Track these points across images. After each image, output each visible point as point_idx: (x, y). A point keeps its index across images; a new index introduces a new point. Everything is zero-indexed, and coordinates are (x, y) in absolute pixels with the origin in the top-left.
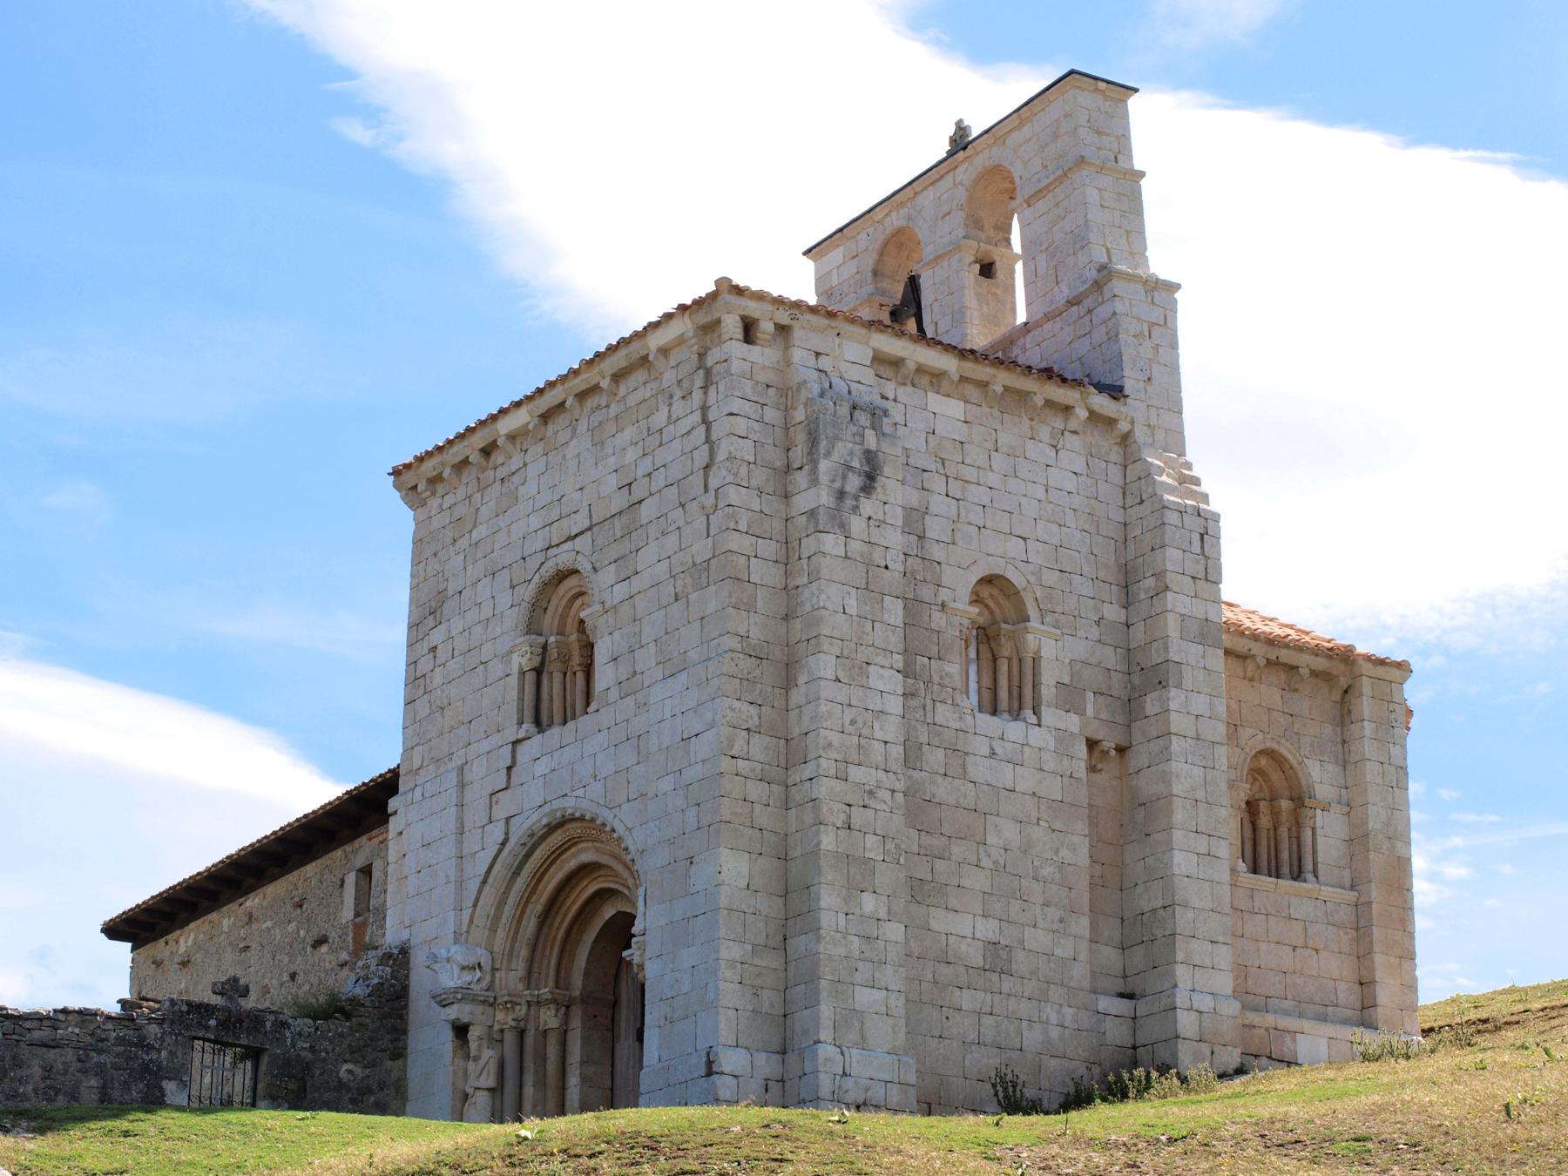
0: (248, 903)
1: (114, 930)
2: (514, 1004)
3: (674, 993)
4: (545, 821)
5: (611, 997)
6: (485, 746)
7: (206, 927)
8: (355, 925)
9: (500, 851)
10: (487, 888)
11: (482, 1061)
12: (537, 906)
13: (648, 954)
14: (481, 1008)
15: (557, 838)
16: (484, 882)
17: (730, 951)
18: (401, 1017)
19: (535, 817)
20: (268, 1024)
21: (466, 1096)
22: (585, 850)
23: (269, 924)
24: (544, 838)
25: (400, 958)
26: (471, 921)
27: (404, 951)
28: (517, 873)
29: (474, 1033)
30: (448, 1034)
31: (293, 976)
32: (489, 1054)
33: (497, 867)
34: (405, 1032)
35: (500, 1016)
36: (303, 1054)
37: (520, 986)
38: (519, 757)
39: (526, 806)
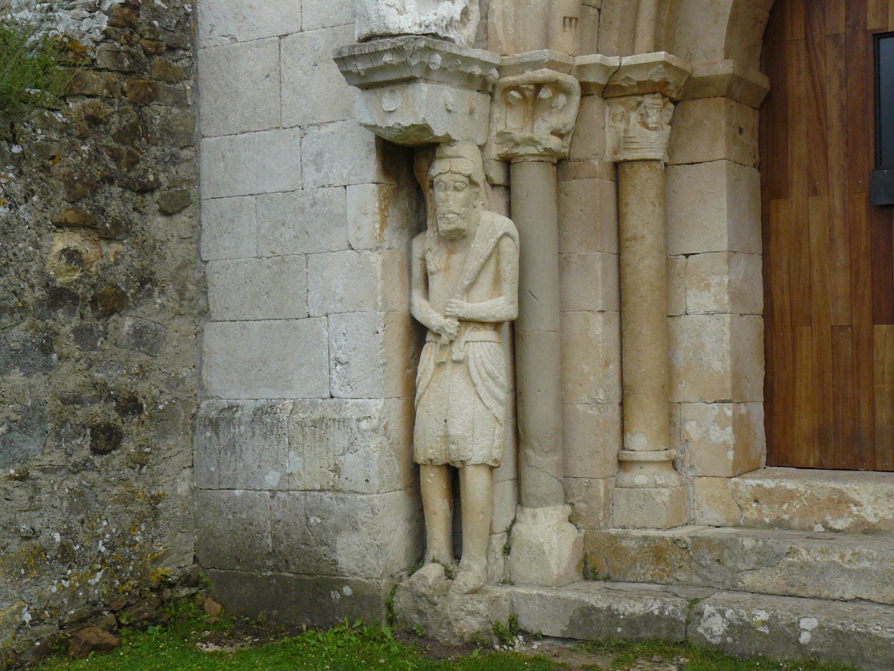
2: (558, 87)
11: (480, 247)
18: (180, 101)
35: (511, 122)
37: (565, 44)
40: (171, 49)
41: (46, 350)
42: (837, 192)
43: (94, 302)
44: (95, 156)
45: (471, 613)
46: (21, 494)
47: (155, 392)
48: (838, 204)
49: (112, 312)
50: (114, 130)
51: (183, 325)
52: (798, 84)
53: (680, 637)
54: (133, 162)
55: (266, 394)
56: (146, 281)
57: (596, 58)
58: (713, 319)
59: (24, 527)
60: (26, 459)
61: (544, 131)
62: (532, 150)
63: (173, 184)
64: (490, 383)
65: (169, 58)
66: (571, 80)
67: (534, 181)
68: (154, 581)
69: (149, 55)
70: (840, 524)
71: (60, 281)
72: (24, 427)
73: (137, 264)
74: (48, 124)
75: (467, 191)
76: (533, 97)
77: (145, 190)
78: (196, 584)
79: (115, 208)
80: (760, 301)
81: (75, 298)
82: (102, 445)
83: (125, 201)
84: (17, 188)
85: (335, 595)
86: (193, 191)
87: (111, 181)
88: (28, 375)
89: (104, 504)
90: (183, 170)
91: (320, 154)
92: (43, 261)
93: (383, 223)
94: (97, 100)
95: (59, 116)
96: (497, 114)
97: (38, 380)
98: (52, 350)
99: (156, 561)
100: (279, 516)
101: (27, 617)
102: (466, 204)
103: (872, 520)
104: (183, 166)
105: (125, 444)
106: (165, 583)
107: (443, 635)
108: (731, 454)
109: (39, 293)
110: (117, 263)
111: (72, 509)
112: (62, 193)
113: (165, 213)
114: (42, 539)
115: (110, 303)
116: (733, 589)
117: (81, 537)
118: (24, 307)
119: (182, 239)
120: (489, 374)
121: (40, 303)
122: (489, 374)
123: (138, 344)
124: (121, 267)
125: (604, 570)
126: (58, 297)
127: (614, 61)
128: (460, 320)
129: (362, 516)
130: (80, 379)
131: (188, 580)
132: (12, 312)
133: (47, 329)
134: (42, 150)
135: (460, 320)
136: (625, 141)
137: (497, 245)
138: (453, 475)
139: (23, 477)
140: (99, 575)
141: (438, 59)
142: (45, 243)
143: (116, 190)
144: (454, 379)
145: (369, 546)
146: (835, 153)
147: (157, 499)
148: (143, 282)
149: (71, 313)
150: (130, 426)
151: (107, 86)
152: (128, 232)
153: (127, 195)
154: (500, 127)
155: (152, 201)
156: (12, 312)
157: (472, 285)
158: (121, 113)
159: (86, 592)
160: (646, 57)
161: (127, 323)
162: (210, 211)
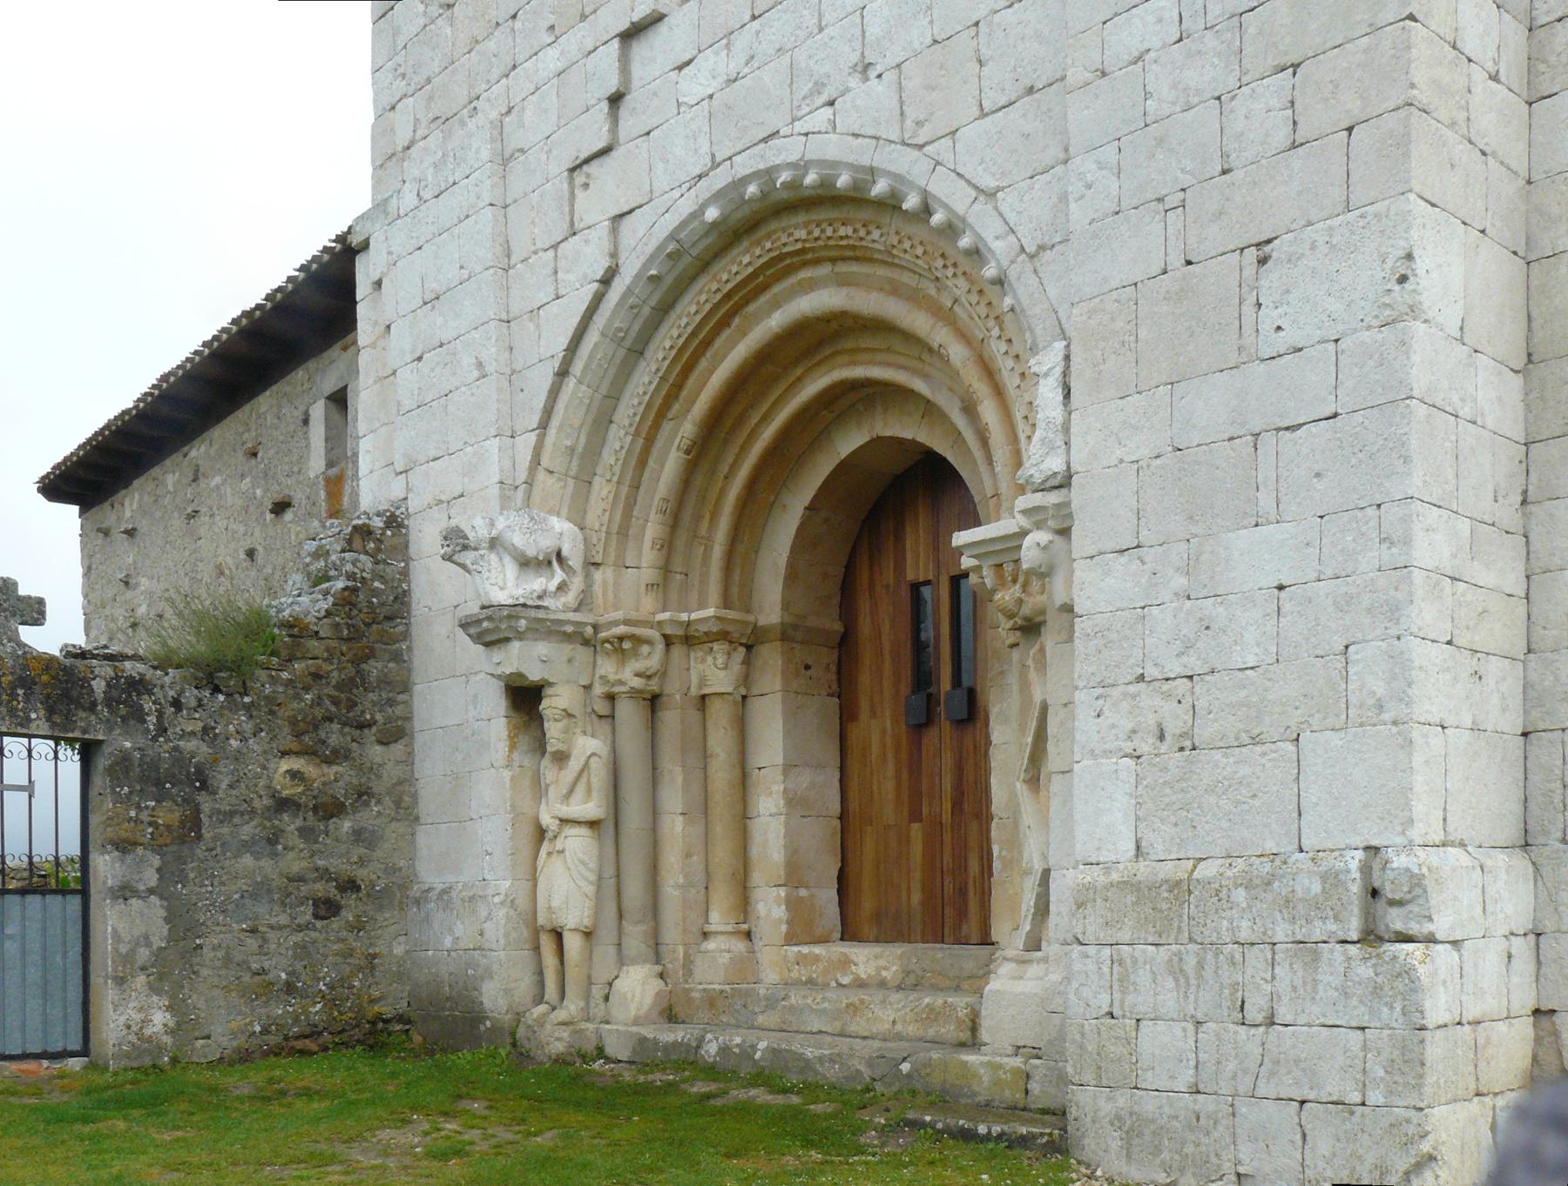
0: (193, 453)
1: (58, 486)
2: (638, 640)
3: (1194, 664)
4: (712, 214)
5: (838, 627)
6: (551, 60)
7: (150, 486)
8: (328, 481)
9: (598, 299)
10: (570, 384)
11: (574, 765)
12: (686, 428)
13: (1081, 541)
14: (567, 649)
15: (742, 262)
16: (563, 373)
17: (1435, 542)
18: (397, 657)
19: (686, 206)
20: (99, 686)
21: (541, 833)
22: (811, 286)
23: (218, 479)
24: (704, 264)
25: (383, 538)
26: (536, 460)
27: (394, 522)
28: (637, 351)
29: (551, 705)
30: (495, 704)
31: (251, 554)
32: (588, 746)
33: (593, 337)
34: (406, 687)
35: (607, 667)
36: (189, 745)
37: (648, 603)
38: (637, 71)
39: (662, 182)
40: (389, 618)
41: (272, 841)
42: (888, 713)
43: (315, 809)
44: (318, 702)
45: (557, 1039)
46: (252, 943)
47: (374, 877)
48: (889, 723)
49: (332, 816)
50: (334, 682)
51: (400, 827)
52: (865, 626)
53: (691, 1058)
54: (352, 705)
55: (451, 879)
56: (363, 795)
57: (666, 616)
58: (781, 817)
59: (255, 966)
60: (256, 918)
61: (628, 675)
62: (623, 689)
63: (388, 720)
64: (582, 868)
65: (387, 626)
66: (653, 634)
67: (628, 712)
68: (370, 1016)
69: (368, 625)
70: (845, 980)
71: (286, 793)
72: (254, 896)
73: (355, 781)
74: (274, 681)
75: (565, 721)
76: (623, 646)
77: (361, 726)
78: (408, 1022)
79: (334, 740)
80: (837, 806)
81: (298, 806)
82: (322, 913)
83: (344, 735)
84: (248, 727)
85: (482, 1028)
86: (407, 725)
87: (331, 720)
88: (257, 859)
89: (325, 956)
90: (399, 710)
91: (476, 696)
92: (270, 779)
93: (512, 747)
94: (319, 662)
95: (285, 675)
96: (599, 662)
97: (267, 864)
98: (277, 842)
99: (372, 1001)
100: (451, 969)
101: (258, 1029)
102: (566, 731)
103: (863, 976)
104: (400, 707)
105: (343, 913)
106: (380, 1018)
107: (539, 1055)
108: (784, 928)
109: (266, 801)
110: (336, 780)
111: (295, 956)
112: (286, 730)
113: (380, 742)
114: (271, 975)
115: (330, 809)
116: (753, 1027)
117: (303, 977)
118: (253, 811)
119: (398, 762)
120: (582, 862)
121: (268, 808)
122: (582, 862)
123: (357, 841)
124: (341, 783)
125: (682, 1016)
126: (283, 804)
127: (684, 617)
128: (561, 820)
129: (495, 967)
130: (304, 864)
131: (401, 1019)
132: (242, 814)
133: (273, 827)
134: (270, 700)
135: (561, 820)
136: (703, 682)
137: (587, 762)
138: (558, 935)
139: (253, 931)
140: (319, 1006)
141: (523, 623)
142: (272, 766)
143: (335, 726)
144: (556, 865)
145: (502, 989)
146: (887, 683)
147: (374, 956)
148: (360, 795)
149: (296, 816)
150: (350, 900)
151: (327, 649)
152: (346, 758)
153: (347, 729)
154: (602, 672)
155: (370, 735)
156: (242, 814)
157: (571, 792)
158: (340, 670)
159: (307, 1017)
160: (706, 613)
161: (347, 825)
162: (420, 740)
